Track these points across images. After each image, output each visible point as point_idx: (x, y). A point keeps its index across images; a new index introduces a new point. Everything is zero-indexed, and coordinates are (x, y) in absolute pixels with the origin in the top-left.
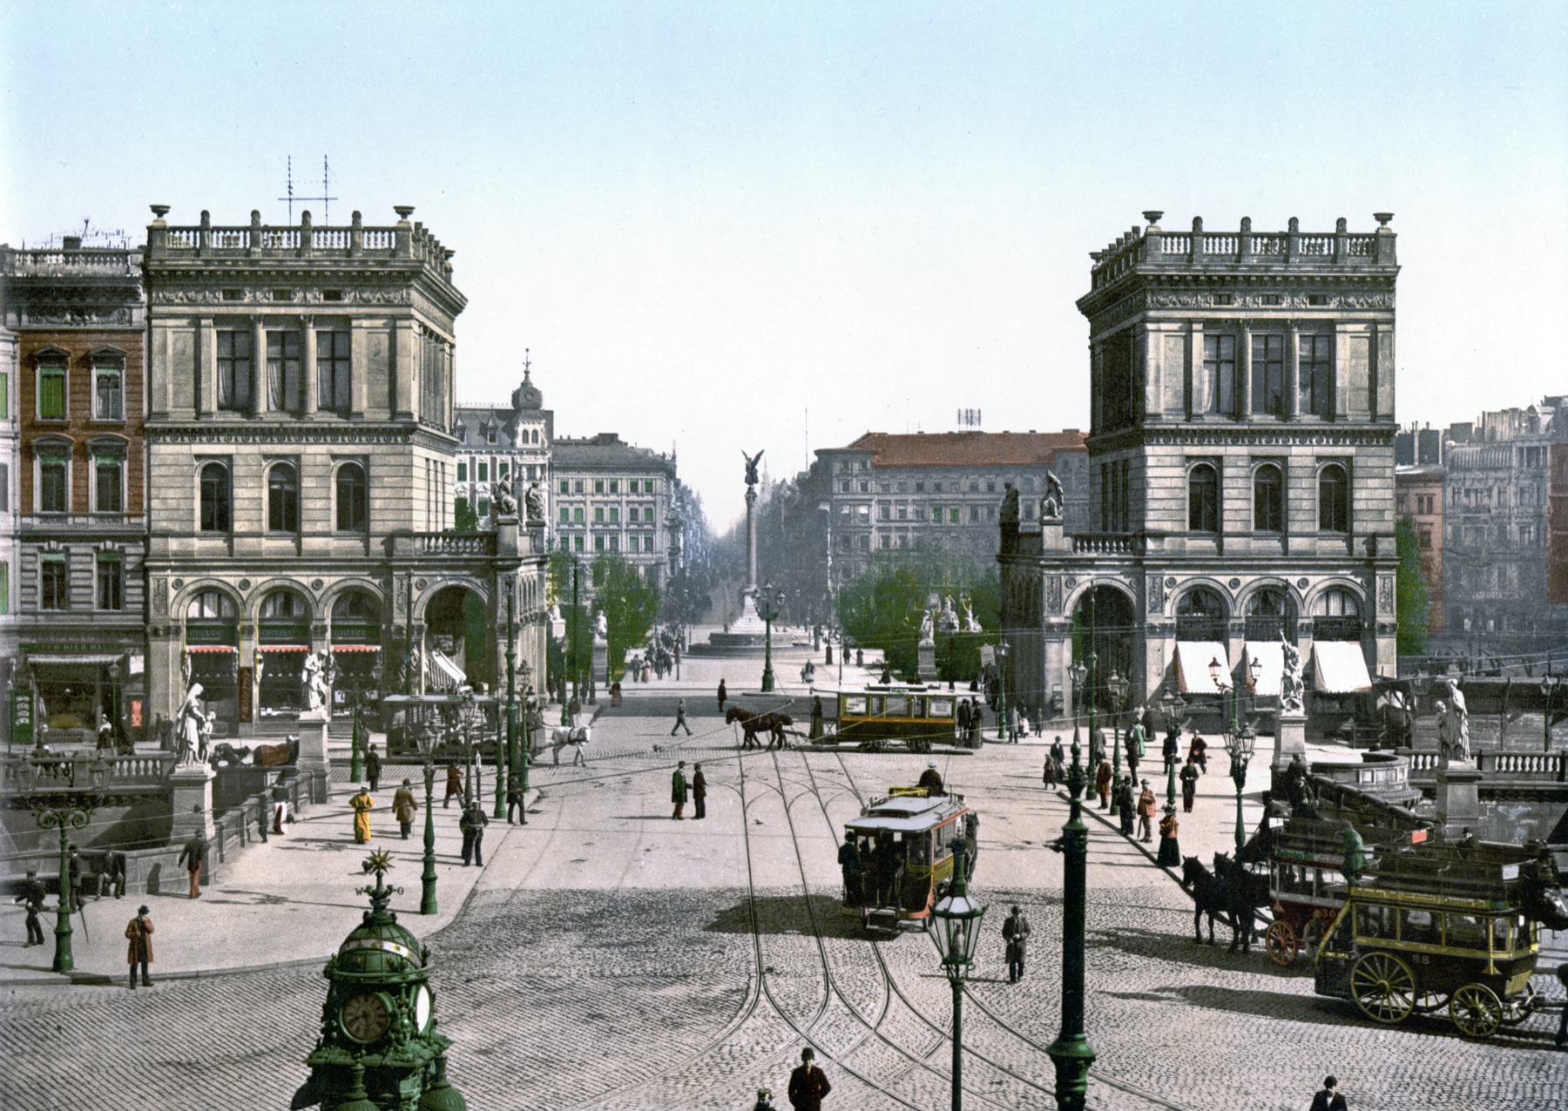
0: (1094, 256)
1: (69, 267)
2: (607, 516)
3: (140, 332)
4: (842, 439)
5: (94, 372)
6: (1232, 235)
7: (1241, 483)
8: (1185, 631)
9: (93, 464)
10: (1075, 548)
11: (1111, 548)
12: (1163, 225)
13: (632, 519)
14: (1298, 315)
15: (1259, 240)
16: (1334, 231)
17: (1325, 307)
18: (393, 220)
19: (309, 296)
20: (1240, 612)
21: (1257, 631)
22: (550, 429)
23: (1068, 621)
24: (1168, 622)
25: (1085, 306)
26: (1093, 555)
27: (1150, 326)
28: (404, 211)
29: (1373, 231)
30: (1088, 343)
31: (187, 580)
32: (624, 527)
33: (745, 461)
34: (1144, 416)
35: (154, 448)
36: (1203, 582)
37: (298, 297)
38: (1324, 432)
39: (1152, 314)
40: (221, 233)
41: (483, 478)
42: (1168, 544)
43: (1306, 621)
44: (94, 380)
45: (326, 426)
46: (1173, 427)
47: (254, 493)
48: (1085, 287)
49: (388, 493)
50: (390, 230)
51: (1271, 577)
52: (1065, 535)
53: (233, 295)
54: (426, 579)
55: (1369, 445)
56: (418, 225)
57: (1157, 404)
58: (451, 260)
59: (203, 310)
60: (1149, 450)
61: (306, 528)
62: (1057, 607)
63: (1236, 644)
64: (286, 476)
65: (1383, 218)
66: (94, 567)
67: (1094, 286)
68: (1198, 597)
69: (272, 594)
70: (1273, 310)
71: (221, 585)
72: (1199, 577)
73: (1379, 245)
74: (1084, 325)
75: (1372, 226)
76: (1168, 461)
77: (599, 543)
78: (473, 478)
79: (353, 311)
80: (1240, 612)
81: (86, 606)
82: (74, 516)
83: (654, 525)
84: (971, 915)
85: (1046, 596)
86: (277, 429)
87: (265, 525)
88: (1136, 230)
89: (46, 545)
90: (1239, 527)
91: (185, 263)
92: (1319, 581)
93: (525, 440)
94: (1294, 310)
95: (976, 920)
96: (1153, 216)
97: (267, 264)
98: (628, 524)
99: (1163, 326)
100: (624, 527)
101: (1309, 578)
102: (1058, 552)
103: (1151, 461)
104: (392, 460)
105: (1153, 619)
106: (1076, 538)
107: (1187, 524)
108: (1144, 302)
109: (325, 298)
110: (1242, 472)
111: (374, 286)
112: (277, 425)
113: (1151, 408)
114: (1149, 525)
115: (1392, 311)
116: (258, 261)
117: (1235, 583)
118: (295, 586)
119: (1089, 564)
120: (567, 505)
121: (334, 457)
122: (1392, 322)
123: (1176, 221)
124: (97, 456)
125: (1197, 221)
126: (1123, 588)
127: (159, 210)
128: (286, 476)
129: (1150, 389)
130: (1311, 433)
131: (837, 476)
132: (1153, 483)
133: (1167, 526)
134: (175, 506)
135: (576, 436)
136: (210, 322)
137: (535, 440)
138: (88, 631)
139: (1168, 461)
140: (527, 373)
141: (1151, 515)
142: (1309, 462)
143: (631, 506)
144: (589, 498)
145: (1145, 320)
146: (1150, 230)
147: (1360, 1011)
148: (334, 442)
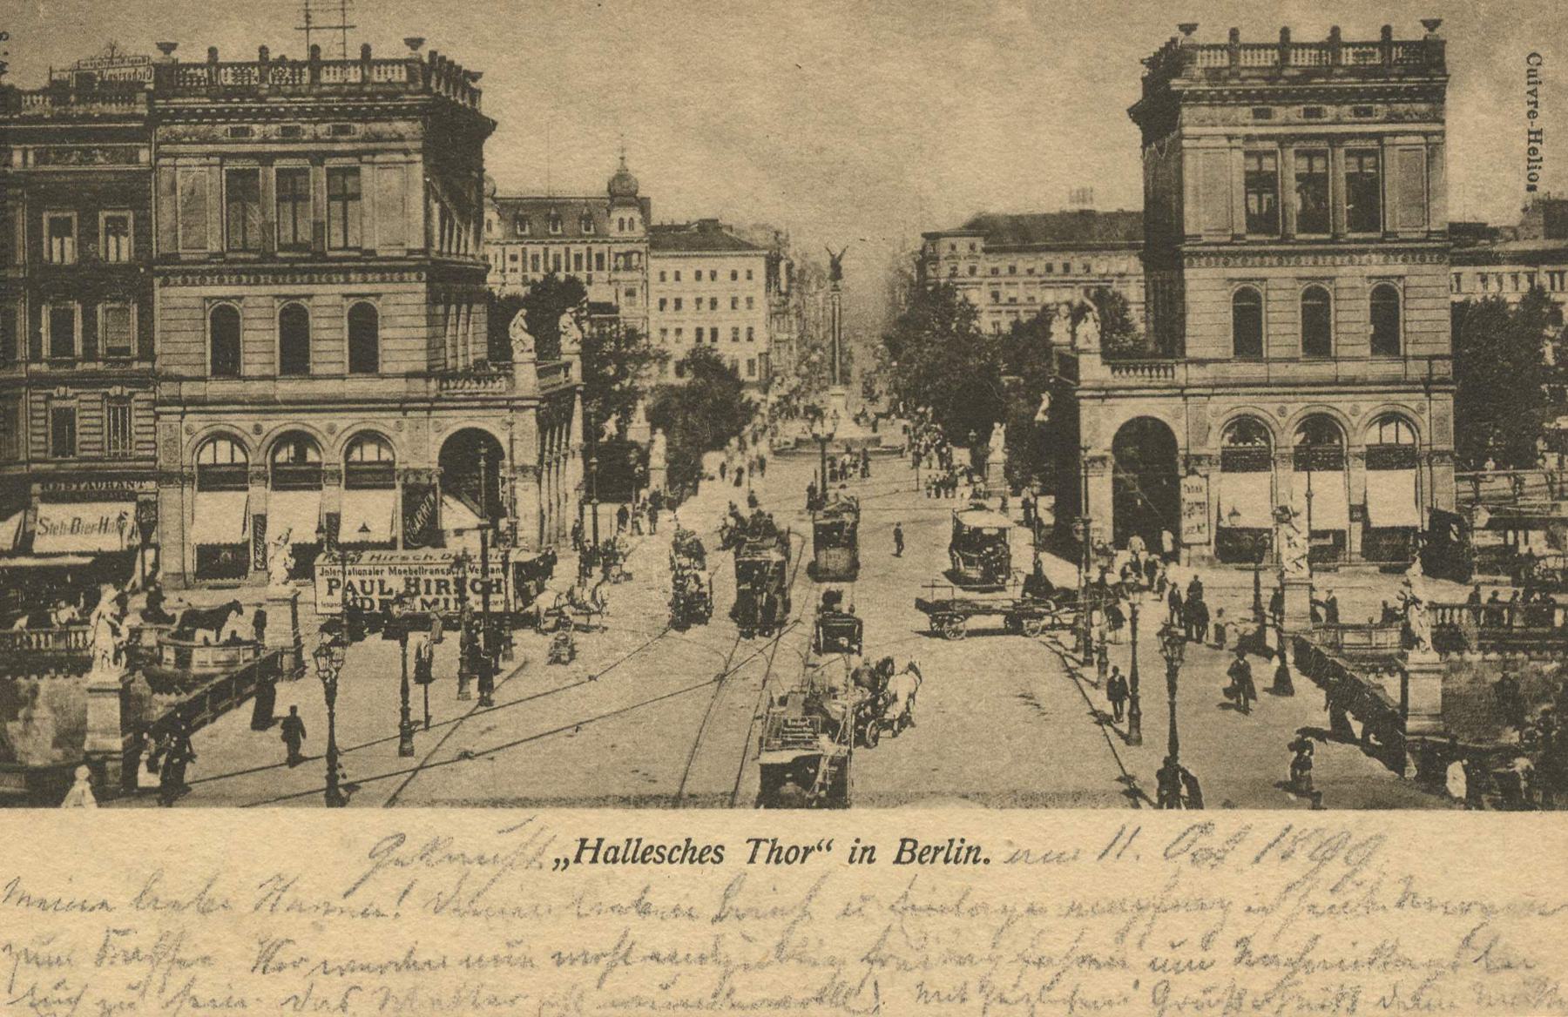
8: (1231, 462)
12: (1199, 37)
20: (1291, 439)
21: (1305, 460)
22: (646, 217)
34: (1183, 238)
35: (171, 291)
41: (600, 268)
49: (399, 333)
51: (1321, 404)
55: (1423, 261)
65: (1432, 25)
68: (1245, 427)
69: (283, 440)
72: (364, 421)
75: (1419, 34)
78: (589, 268)
82: (84, 361)
88: (1174, 41)
90: (1284, 352)
92: (1370, 406)
93: (621, 228)
96: (1188, 29)
107: (1232, 350)
110: (264, 312)
115: (1443, 122)
118: (308, 430)
119: (1130, 392)
122: (1442, 134)
133: (1212, 353)
137: (631, 227)
145: (1182, 137)
147: (488, 504)
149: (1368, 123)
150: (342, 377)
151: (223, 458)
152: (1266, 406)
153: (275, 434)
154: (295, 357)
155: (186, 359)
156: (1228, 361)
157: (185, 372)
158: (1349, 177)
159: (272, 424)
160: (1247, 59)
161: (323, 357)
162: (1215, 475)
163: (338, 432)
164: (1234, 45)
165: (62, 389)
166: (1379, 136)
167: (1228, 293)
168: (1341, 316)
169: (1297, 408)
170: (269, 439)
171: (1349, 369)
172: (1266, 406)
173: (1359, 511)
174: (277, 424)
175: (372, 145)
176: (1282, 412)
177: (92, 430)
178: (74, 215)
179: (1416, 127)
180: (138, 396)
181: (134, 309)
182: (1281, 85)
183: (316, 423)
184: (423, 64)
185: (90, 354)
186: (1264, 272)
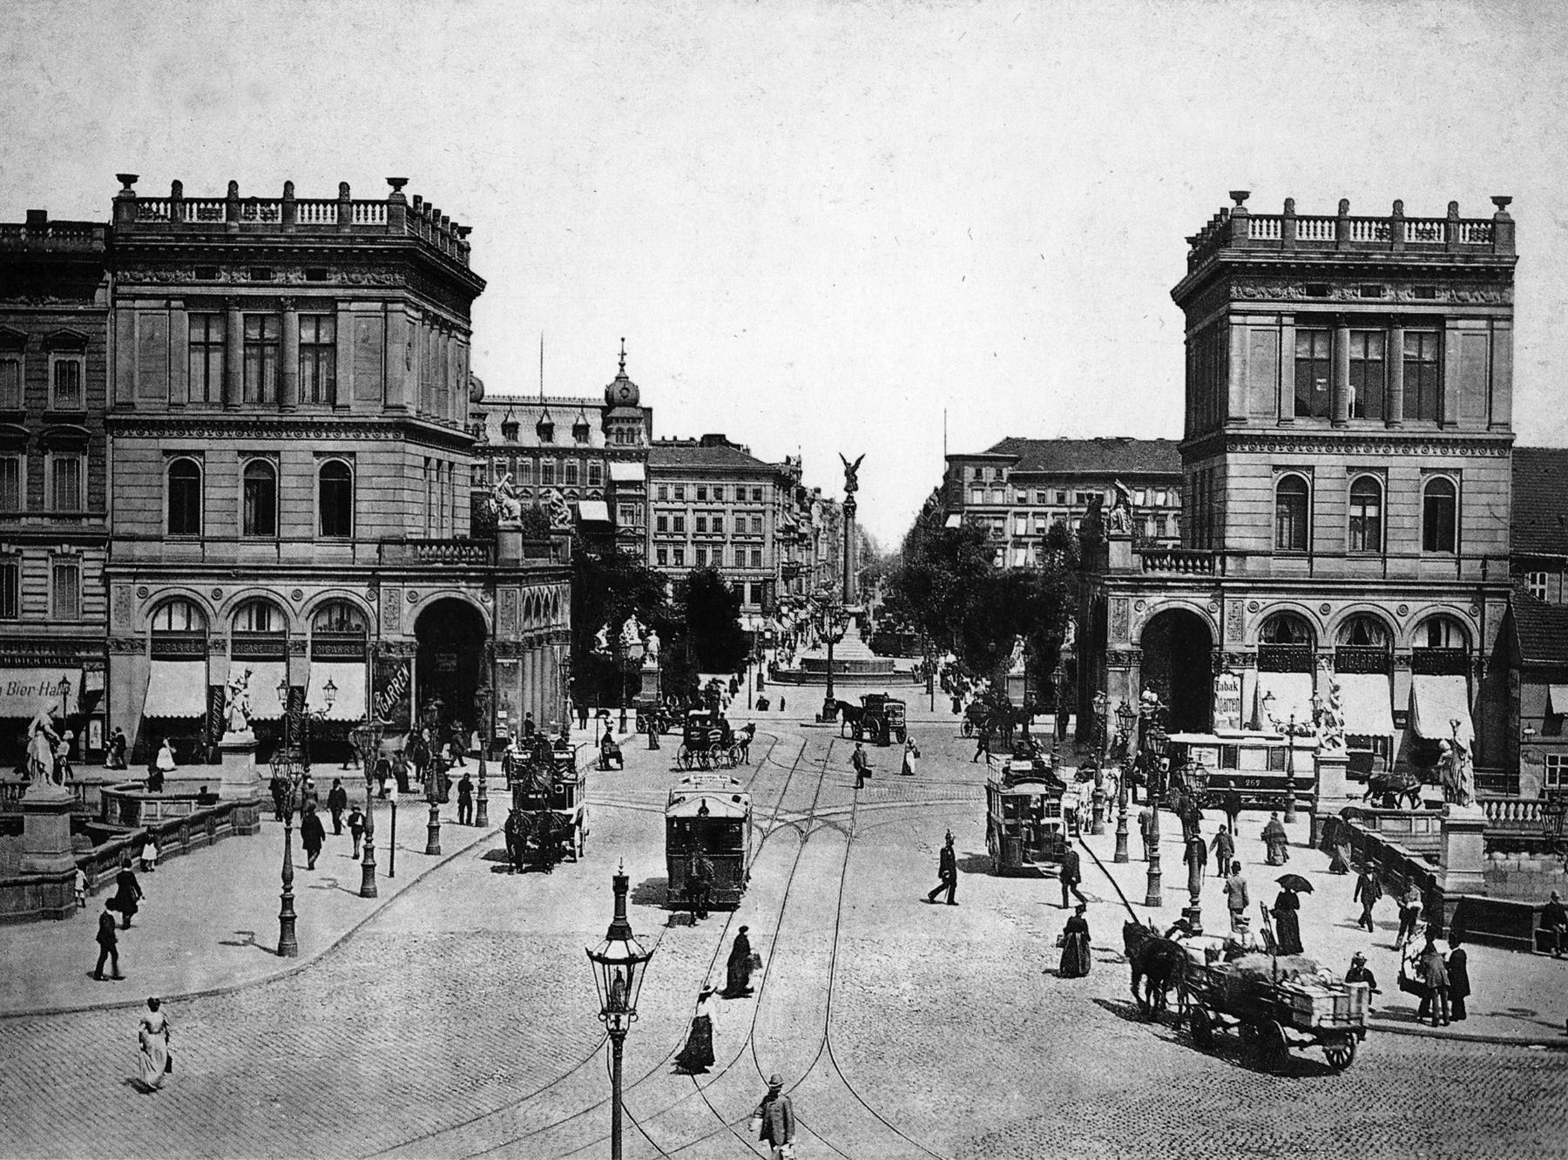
0: (1190, 240)
1: (61, 243)
2: (749, 528)
3: (106, 313)
4: (978, 443)
5: (52, 359)
6: (1330, 219)
7: (1335, 497)
8: (1267, 661)
9: (48, 460)
10: (1145, 566)
11: (1186, 567)
12: (1252, 206)
13: (737, 530)
14: (1400, 309)
15: (195, 206)
16: (1336, 214)
17: (1378, 299)
18: (385, 192)
19: (291, 277)
20: (1329, 640)
23: (1135, 648)
24: (1248, 650)
25: (1182, 296)
26: (1165, 574)
27: (1234, 319)
28: (397, 183)
29: (1491, 217)
30: (1184, 337)
31: (152, 589)
32: (690, 537)
33: (844, 468)
35: (120, 442)
36: (1289, 607)
37: (1389, 295)
38: (1430, 440)
39: (1236, 306)
40: (1468, 227)
42: (1252, 564)
43: (1405, 653)
44: (51, 367)
45: (308, 419)
46: (1259, 432)
47: (229, 493)
48: (1178, 271)
50: (381, 203)
52: (1133, 552)
53: (207, 274)
54: (416, 590)
56: (417, 199)
57: (1242, 408)
58: (468, 238)
59: (173, 290)
60: (1230, 456)
61: (1393, 548)
62: (1122, 632)
63: (1403, 677)
64: (1366, 488)
65: (1501, 202)
66: (50, 573)
67: (1190, 269)
68: (1361, 626)
69: (325, 607)
70: (1377, 303)
71: (189, 594)
73: (1499, 230)
74: (1178, 317)
75: (1490, 211)
76: (1252, 471)
77: (701, 555)
79: (340, 292)
80: (1329, 640)
81: (42, 615)
83: (762, 537)
84: (631, 961)
85: (1110, 620)
86: (254, 422)
87: (317, 529)
88: (1225, 211)
89: (58, 549)
90: (1332, 547)
91: (153, 238)
94: (1398, 304)
95: (639, 966)
96: (1240, 196)
97: (242, 242)
98: (734, 536)
99: (1250, 319)
100: (729, 538)
101: (303, 589)
102: (1125, 571)
103: (1232, 471)
104: (383, 458)
105: (1231, 647)
106: (1144, 555)
107: (166, 526)
108: (1229, 292)
109: (197, 277)
110: (1336, 485)
111: (362, 265)
112: (254, 419)
113: (1233, 411)
114: (1231, 543)
115: (1511, 306)
116: (235, 236)
117: (1403, 611)
119: (1160, 586)
120: (665, 514)
121: (317, 454)
122: (1510, 318)
123: (1264, 202)
124: (54, 451)
125: (1289, 203)
126: (1462, 616)
127: (127, 180)
128: (1366, 488)
129: (1234, 389)
130: (1416, 442)
131: (971, 485)
132: (1233, 494)
133: (1250, 544)
134: (140, 507)
135: (683, 437)
136: (180, 303)
138: (42, 643)
139: (1252, 471)
140: (622, 365)
141: (1231, 532)
142: (153, 456)
143: (699, 514)
144: (691, 506)
146: (1498, 217)
148: (318, 438)
149: (1430, 304)
150: (309, 540)
151: (179, 623)
152: (1309, 604)
153: (236, 599)
154: (264, 519)
155: (141, 517)
156: (1270, 554)
157: (140, 530)
158: (1408, 362)
159: (234, 589)
160: (1302, 234)
161: (293, 518)
162: (1251, 674)
163: (306, 597)
164: (1288, 216)
165: (66, 547)
166: (333, 301)
167: (1272, 483)
168: (1412, 510)
169: (1341, 606)
170: (310, 606)
171: (290, 551)
172: (1309, 604)
173: (1405, 718)
174: (236, 590)
175: (350, 292)
176: (1326, 610)
177: (33, 590)
178: (52, 359)
179: (374, 293)
180: (87, 555)
181: (84, 461)
182: (1337, 260)
183: (282, 589)
184: (408, 208)
185: (35, 510)
186: (1310, 460)
